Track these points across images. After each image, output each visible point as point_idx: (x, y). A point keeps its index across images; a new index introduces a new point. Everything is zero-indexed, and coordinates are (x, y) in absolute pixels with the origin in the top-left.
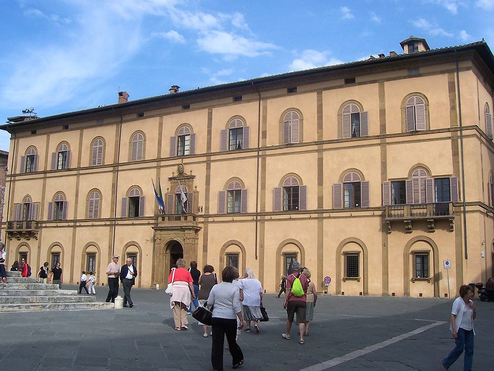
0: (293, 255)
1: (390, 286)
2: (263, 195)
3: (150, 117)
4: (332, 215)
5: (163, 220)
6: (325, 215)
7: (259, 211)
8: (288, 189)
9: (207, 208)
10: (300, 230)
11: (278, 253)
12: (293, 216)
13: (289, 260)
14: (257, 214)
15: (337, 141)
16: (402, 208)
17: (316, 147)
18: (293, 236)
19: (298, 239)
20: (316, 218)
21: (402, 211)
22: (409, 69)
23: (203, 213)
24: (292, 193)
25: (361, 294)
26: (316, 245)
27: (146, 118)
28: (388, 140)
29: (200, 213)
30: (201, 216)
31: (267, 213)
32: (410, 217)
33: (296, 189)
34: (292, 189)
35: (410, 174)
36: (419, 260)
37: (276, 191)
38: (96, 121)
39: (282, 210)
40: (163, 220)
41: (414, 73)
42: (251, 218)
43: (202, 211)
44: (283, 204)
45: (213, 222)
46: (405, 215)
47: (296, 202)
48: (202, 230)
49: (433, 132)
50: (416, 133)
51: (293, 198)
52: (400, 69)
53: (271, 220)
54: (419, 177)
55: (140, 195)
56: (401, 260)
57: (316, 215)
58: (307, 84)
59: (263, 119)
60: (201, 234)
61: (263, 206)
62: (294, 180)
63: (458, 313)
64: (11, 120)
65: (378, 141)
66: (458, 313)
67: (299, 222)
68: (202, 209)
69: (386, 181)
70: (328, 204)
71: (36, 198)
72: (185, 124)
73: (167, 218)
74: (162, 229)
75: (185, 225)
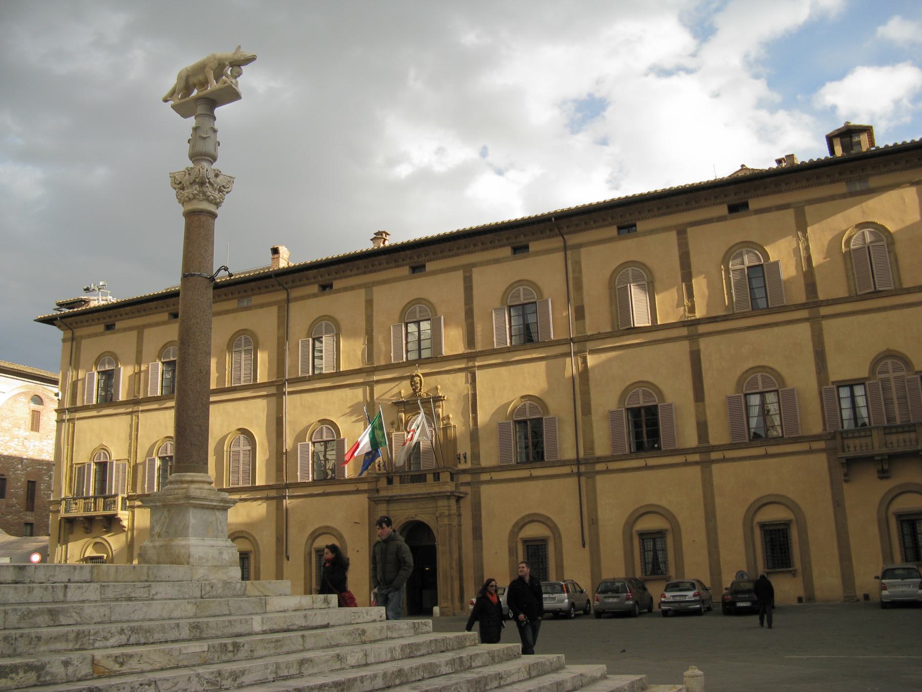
0: (657, 535)
1: (858, 581)
2: (589, 425)
3: (346, 289)
4: (730, 454)
5: (390, 482)
6: (714, 456)
7: (582, 454)
8: (635, 413)
9: (476, 456)
10: (666, 487)
11: (514, 533)
12: (652, 462)
13: (650, 545)
14: (578, 462)
15: (725, 318)
16: (868, 433)
17: (684, 331)
18: (652, 499)
19: (664, 503)
20: (696, 463)
21: (868, 440)
22: (849, 181)
23: (468, 465)
24: (643, 418)
25: (800, 600)
26: (701, 513)
27: (339, 291)
28: (824, 311)
29: (462, 466)
30: (464, 471)
31: (598, 458)
32: (885, 450)
33: (652, 411)
34: (643, 412)
35: (872, 370)
36: (907, 530)
37: (613, 416)
38: (236, 301)
39: (627, 451)
40: (390, 482)
41: (858, 187)
42: (566, 470)
43: (466, 462)
44: (626, 441)
45: (491, 481)
46: (876, 444)
47: (654, 434)
48: (469, 497)
49: (909, 291)
50: (877, 294)
51: (645, 428)
52: (833, 182)
53: (608, 471)
54: (891, 375)
55: (656, 401)
56: (874, 530)
57: (696, 457)
58: (655, 216)
59: (574, 285)
60: (466, 505)
61: (590, 446)
62: (646, 395)
63: (665, 614)
64: (61, 305)
65: (804, 314)
66: (665, 614)
67: (661, 473)
68: (465, 457)
69: (828, 385)
70: (718, 434)
71: (117, 453)
72: (418, 301)
73: (396, 480)
74: (390, 500)
75: (436, 489)
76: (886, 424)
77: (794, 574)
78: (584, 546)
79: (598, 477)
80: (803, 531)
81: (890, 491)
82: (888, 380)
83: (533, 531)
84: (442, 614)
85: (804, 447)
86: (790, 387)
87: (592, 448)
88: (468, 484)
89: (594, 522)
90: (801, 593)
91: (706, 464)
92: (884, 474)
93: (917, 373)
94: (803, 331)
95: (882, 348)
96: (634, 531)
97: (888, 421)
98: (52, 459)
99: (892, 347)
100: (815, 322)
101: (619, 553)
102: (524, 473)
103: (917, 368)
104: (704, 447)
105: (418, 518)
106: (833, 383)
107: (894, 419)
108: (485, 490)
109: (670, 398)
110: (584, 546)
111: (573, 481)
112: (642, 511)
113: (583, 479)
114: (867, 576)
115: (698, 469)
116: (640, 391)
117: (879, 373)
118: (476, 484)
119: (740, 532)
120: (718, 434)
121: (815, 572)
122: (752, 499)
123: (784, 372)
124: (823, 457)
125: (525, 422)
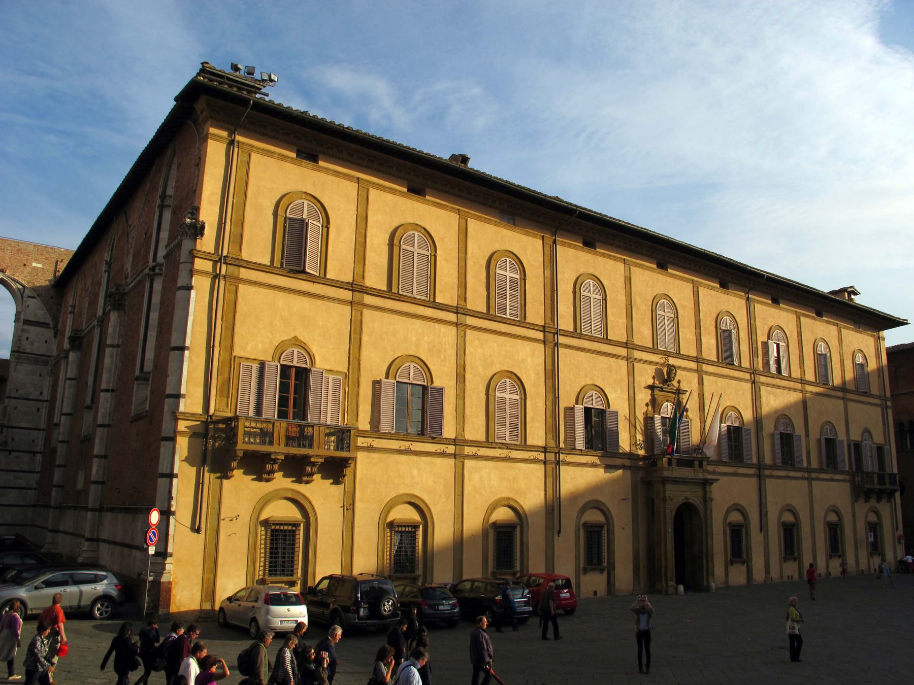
42: (533, 455)
78: (761, 531)
102: (404, 445)
112: (603, 507)
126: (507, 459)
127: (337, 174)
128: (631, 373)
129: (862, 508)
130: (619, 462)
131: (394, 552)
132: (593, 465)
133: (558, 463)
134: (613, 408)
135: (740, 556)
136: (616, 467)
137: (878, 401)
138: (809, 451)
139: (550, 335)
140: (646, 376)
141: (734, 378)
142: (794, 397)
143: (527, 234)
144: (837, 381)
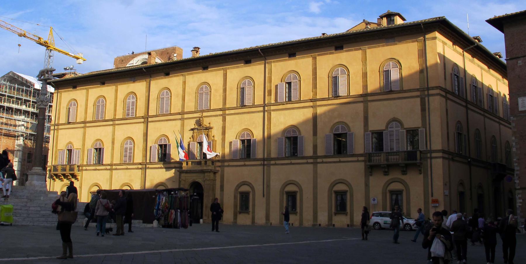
4: (325, 160)
14: (264, 160)
17: (311, 104)
18: (293, 178)
19: (297, 180)
21: (380, 158)
25: (348, 225)
33: (344, 135)
34: (292, 138)
36: (290, 199)
42: (259, 163)
45: (229, 166)
48: (220, 173)
49: (405, 91)
57: (311, 161)
60: (218, 176)
61: (269, 153)
76: (389, 151)
77: (346, 214)
78: (264, 196)
79: (272, 167)
80: (352, 196)
81: (387, 181)
82: (393, 131)
83: (291, 188)
84: (204, 222)
85: (355, 159)
86: (352, 132)
87: (270, 154)
88: (220, 166)
89: (268, 186)
90: (349, 223)
91: (315, 163)
92: (386, 173)
93: (405, 129)
94: (142, 126)
95: (392, 116)
96: (334, 190)
97: (391, 149)
98: (521, 109)
99: (396, 117)
100: (147, 123)
101: (326, 200)
102: (242, 163)
103: (405, 127)
104: (315, 157)
105: (197, 181)
106: (370, 131)
107: (393, 149)
108: (226, 169)
109: (303, 133)
110: (264, 196)
111: (261, 168)
112: (291, 182)
113: (265, 167)
114: (323, 218)
115: (311, 166)
116: (340, 126)
117: (390, 128)
118: (222, 167)
119: (326, 195)
120: (321, 152)
121: (355, 215)
122: (332, 181)
123: (350, 125)
124: (363, 163)
125: (244, 140)
126: (127, 169)
127: (215, 70)
128: (183, 125)
129: (378, 183)
130: (172, 165)
131: (339, 202)
132: (161, 168)
133: (146, 168)
134: (302, 135)
135: (247, 208)
136: (171, 168)
137: (142, 120)
138: (359, 144)
139: (146, 119)
140: (191, 124)
141: (170, 120)
142: (308, 113)
143: (407, 43)
144: (357, 90)
